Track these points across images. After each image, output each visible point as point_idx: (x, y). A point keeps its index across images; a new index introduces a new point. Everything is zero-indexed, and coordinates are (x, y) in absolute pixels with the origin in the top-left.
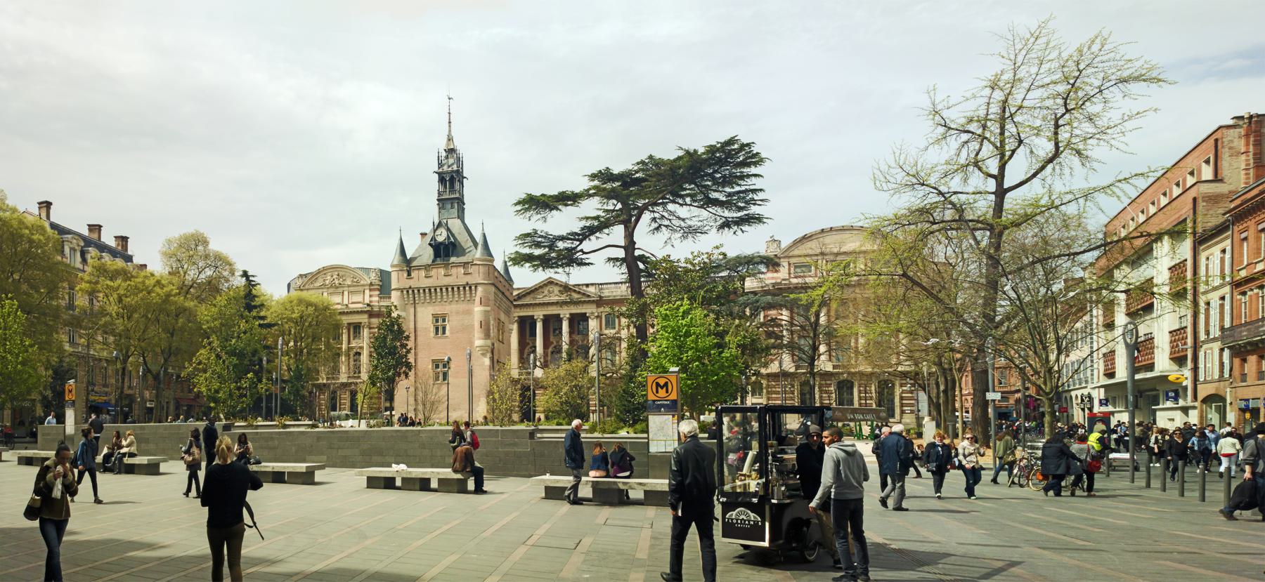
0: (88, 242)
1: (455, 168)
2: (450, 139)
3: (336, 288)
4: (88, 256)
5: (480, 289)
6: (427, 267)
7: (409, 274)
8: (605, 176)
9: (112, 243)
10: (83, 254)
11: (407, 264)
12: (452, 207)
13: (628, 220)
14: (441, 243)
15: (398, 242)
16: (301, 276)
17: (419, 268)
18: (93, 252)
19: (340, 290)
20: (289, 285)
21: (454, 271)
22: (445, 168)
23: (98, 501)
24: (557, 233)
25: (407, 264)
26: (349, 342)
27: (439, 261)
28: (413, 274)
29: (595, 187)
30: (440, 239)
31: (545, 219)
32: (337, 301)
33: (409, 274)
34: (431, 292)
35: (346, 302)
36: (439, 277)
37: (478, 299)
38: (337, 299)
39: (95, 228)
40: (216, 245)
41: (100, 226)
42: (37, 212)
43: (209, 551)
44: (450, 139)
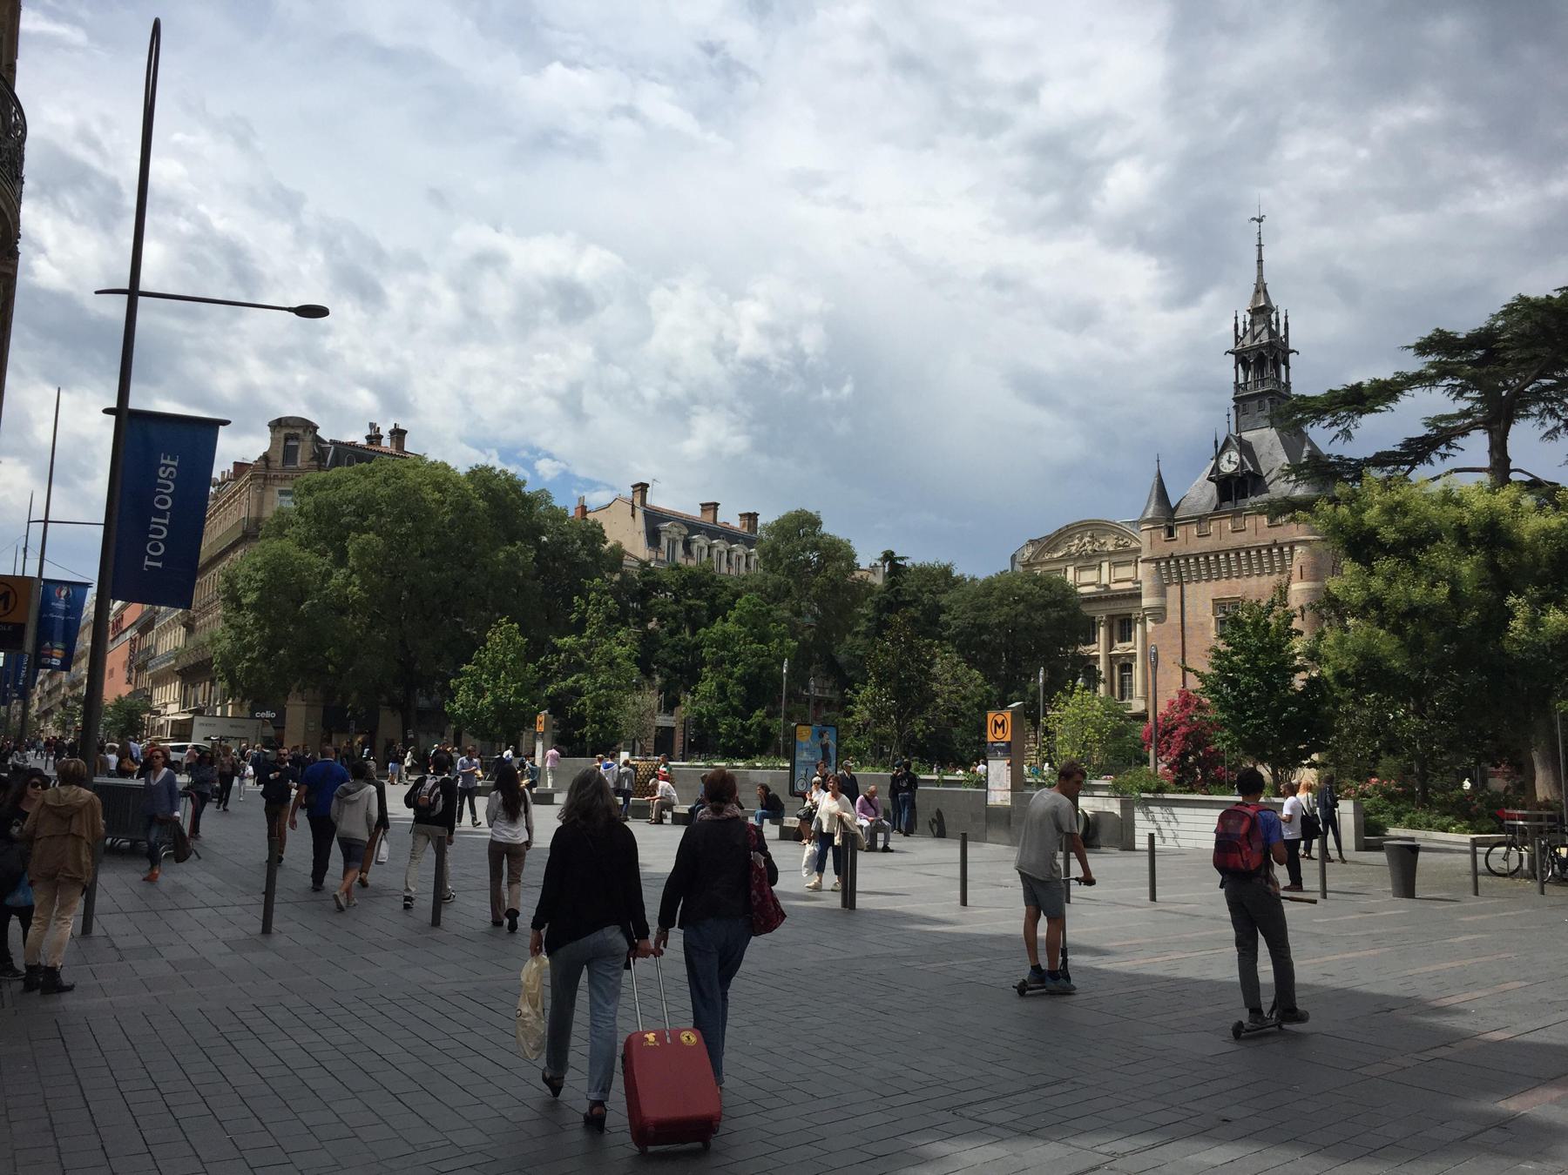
0: (693, 527)
1: (1265, 338)
2: (1261, 289)
3: (1088, 560)
4: (694, 548)
5: (1299, 549)
6: (1201, 519)
7: (1171, 533)
8: (1439, 343)
9: (736, 523)
10: (687, 545)
11: (1167, 516)
12: (1261, 409)
13: (1498, 420)
14: (1230, 476)
15: (1153, 480)
16: (1032, 542)
17: (1187, 521)
18: (700, 540)
19: (1096, 562)
20: (1013, 558)
21: (1250, 523)
22: (1248, 342)
23: (1344, 862)
24: (1360, 456)
25: (1167, 516)
26: (1111, 646)
27: (1228, 506)
28: (1177, 534)
29: (1432, 365)
30: (1227, 468)
31: (1347, 434)
32: (1085, 581)
33: (1171, 533)
34: (1211, 564)
35: (1105, 580)
36: (1223, 535)
37: (1296, 569)
38: (1089, 576)
39: (712, 507)
40: (829, 528)
41: (716, 505)
42: (630, 495)
43: (1237, 979)
44: (1261, 289)
